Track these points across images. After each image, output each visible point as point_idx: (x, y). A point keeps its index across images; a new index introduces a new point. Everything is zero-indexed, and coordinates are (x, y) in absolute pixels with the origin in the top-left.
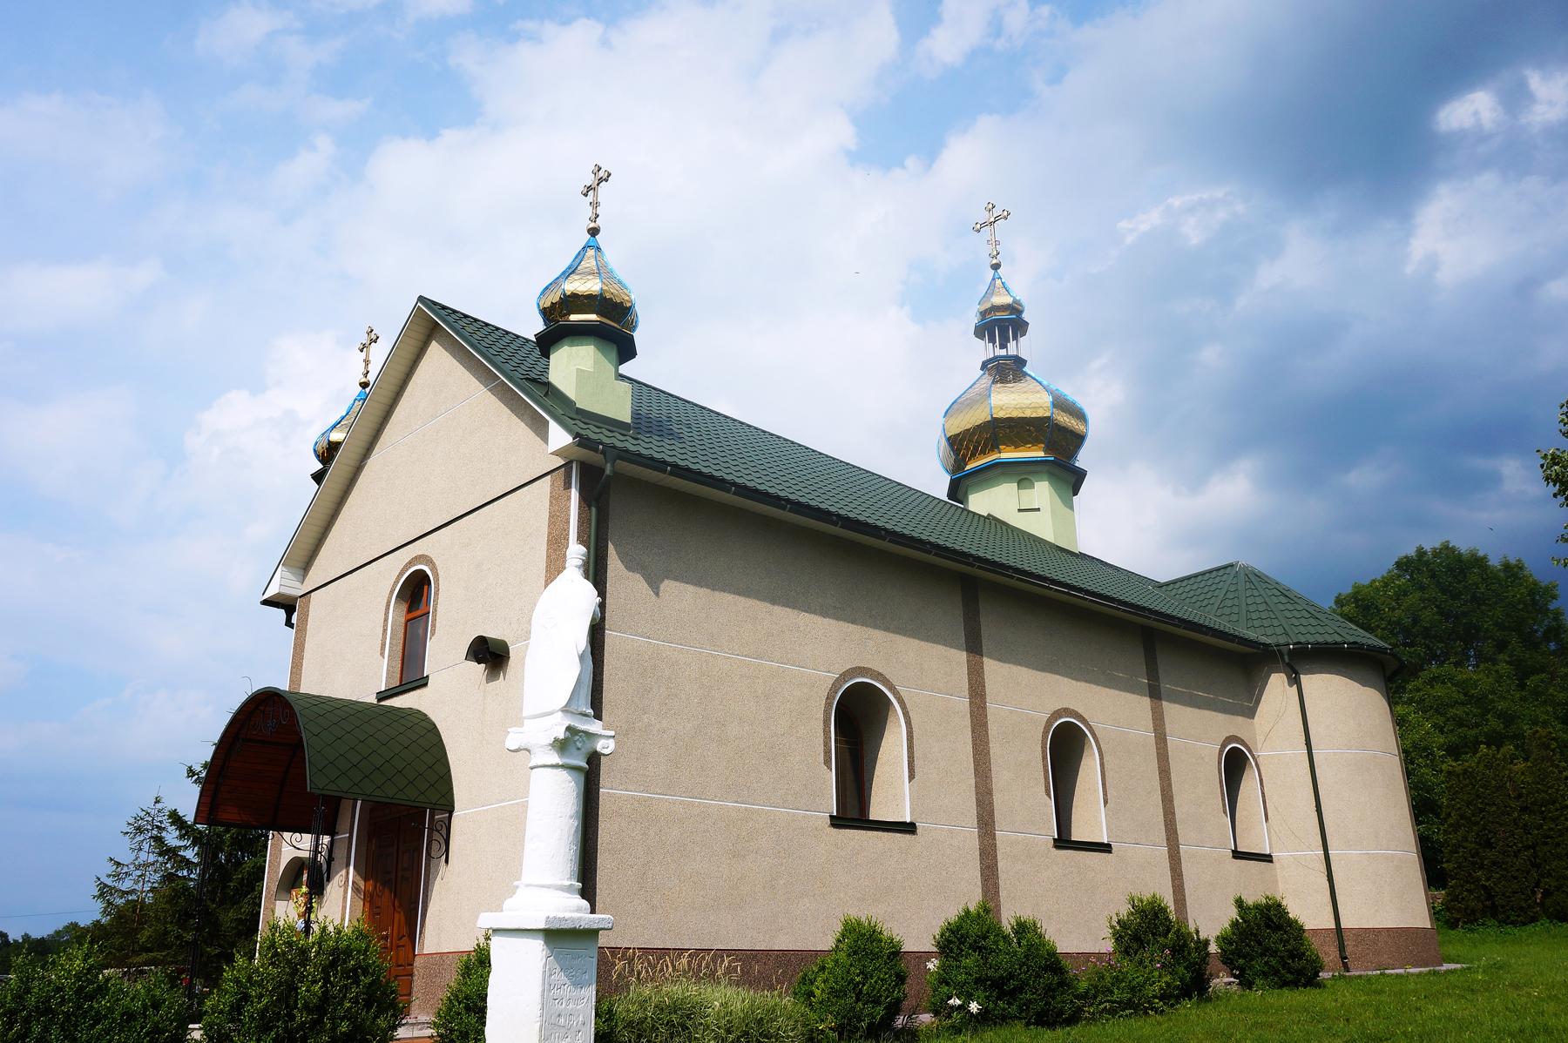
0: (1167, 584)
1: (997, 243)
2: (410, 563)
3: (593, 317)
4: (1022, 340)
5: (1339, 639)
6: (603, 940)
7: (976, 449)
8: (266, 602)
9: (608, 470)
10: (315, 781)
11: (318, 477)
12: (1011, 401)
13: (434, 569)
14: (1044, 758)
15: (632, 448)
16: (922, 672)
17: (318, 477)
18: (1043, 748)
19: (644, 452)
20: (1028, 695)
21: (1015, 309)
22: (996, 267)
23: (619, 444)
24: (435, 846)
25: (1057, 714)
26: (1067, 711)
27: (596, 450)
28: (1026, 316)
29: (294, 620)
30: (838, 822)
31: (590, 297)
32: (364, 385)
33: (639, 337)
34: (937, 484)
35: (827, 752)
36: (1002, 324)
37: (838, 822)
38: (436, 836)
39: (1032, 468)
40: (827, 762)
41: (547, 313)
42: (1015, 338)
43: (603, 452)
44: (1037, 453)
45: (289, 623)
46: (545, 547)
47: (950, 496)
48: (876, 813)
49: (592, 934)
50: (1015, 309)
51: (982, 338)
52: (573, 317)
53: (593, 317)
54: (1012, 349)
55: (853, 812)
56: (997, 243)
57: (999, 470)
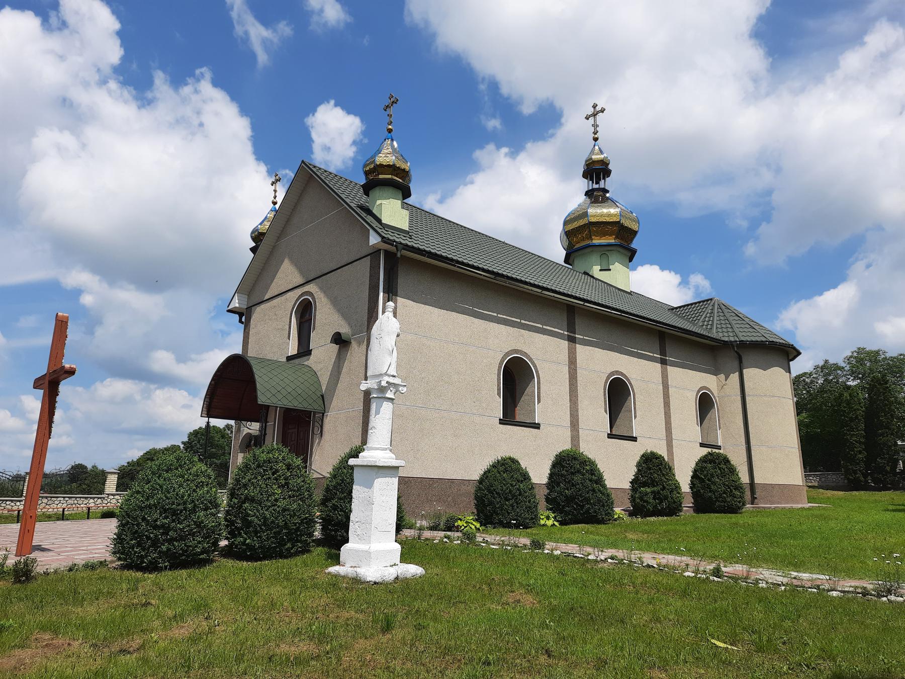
0: (676, 308)
1: (597, 126)
2: (302, 295)
3: (390, 176)
4: (607, 179)
5: (764, 339)
6: (402, 473)
7: (581, 237)
8: (229, 311)
9: (399, 255)
10: (262, 399)
11: (253, 250)
12: (599, 212)
13: (314, 298)
14: (605, 395)
15: (409, 244)
16: (545, 350)
17: (253, 250)
18: (605, 389)
19: (415, 246)
20: (599, 362)
21: (604, 163)
22: (596, 139)
23: (403, 242)
24: (316, 429)
25: (612, 373)
26: (617, 372)
27: (392, 245)
28: (610, 167)
29: (243, 319)
30: (502, 422)
31: (389, 166)
32: (275, 203)
33: (412, 187)
34: (557, 253)
35: (499, 389)
36: (596, 171)
37: (502, 422)
38: (316, 424)
39: (609, 248)
40: (499, 394)
41: (367, 173)
42: (604, 178)
43: (396, 246)
44: (611, 240)
45: (240, 321)
46: (367, 291)
47: (566, 261)
48: (519, 418)
49: (397, 468)
50: (604, 163)
51: (586, 178)
52: (381, 176)
53: (390, 176)
54: (602, 184)
55: (508, 418)
56: (597, 126)
57: (590, 249)
